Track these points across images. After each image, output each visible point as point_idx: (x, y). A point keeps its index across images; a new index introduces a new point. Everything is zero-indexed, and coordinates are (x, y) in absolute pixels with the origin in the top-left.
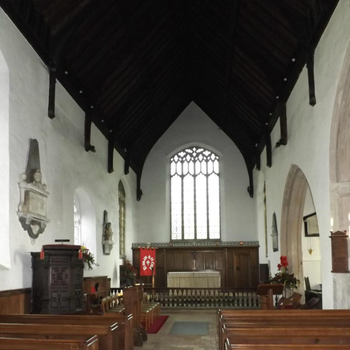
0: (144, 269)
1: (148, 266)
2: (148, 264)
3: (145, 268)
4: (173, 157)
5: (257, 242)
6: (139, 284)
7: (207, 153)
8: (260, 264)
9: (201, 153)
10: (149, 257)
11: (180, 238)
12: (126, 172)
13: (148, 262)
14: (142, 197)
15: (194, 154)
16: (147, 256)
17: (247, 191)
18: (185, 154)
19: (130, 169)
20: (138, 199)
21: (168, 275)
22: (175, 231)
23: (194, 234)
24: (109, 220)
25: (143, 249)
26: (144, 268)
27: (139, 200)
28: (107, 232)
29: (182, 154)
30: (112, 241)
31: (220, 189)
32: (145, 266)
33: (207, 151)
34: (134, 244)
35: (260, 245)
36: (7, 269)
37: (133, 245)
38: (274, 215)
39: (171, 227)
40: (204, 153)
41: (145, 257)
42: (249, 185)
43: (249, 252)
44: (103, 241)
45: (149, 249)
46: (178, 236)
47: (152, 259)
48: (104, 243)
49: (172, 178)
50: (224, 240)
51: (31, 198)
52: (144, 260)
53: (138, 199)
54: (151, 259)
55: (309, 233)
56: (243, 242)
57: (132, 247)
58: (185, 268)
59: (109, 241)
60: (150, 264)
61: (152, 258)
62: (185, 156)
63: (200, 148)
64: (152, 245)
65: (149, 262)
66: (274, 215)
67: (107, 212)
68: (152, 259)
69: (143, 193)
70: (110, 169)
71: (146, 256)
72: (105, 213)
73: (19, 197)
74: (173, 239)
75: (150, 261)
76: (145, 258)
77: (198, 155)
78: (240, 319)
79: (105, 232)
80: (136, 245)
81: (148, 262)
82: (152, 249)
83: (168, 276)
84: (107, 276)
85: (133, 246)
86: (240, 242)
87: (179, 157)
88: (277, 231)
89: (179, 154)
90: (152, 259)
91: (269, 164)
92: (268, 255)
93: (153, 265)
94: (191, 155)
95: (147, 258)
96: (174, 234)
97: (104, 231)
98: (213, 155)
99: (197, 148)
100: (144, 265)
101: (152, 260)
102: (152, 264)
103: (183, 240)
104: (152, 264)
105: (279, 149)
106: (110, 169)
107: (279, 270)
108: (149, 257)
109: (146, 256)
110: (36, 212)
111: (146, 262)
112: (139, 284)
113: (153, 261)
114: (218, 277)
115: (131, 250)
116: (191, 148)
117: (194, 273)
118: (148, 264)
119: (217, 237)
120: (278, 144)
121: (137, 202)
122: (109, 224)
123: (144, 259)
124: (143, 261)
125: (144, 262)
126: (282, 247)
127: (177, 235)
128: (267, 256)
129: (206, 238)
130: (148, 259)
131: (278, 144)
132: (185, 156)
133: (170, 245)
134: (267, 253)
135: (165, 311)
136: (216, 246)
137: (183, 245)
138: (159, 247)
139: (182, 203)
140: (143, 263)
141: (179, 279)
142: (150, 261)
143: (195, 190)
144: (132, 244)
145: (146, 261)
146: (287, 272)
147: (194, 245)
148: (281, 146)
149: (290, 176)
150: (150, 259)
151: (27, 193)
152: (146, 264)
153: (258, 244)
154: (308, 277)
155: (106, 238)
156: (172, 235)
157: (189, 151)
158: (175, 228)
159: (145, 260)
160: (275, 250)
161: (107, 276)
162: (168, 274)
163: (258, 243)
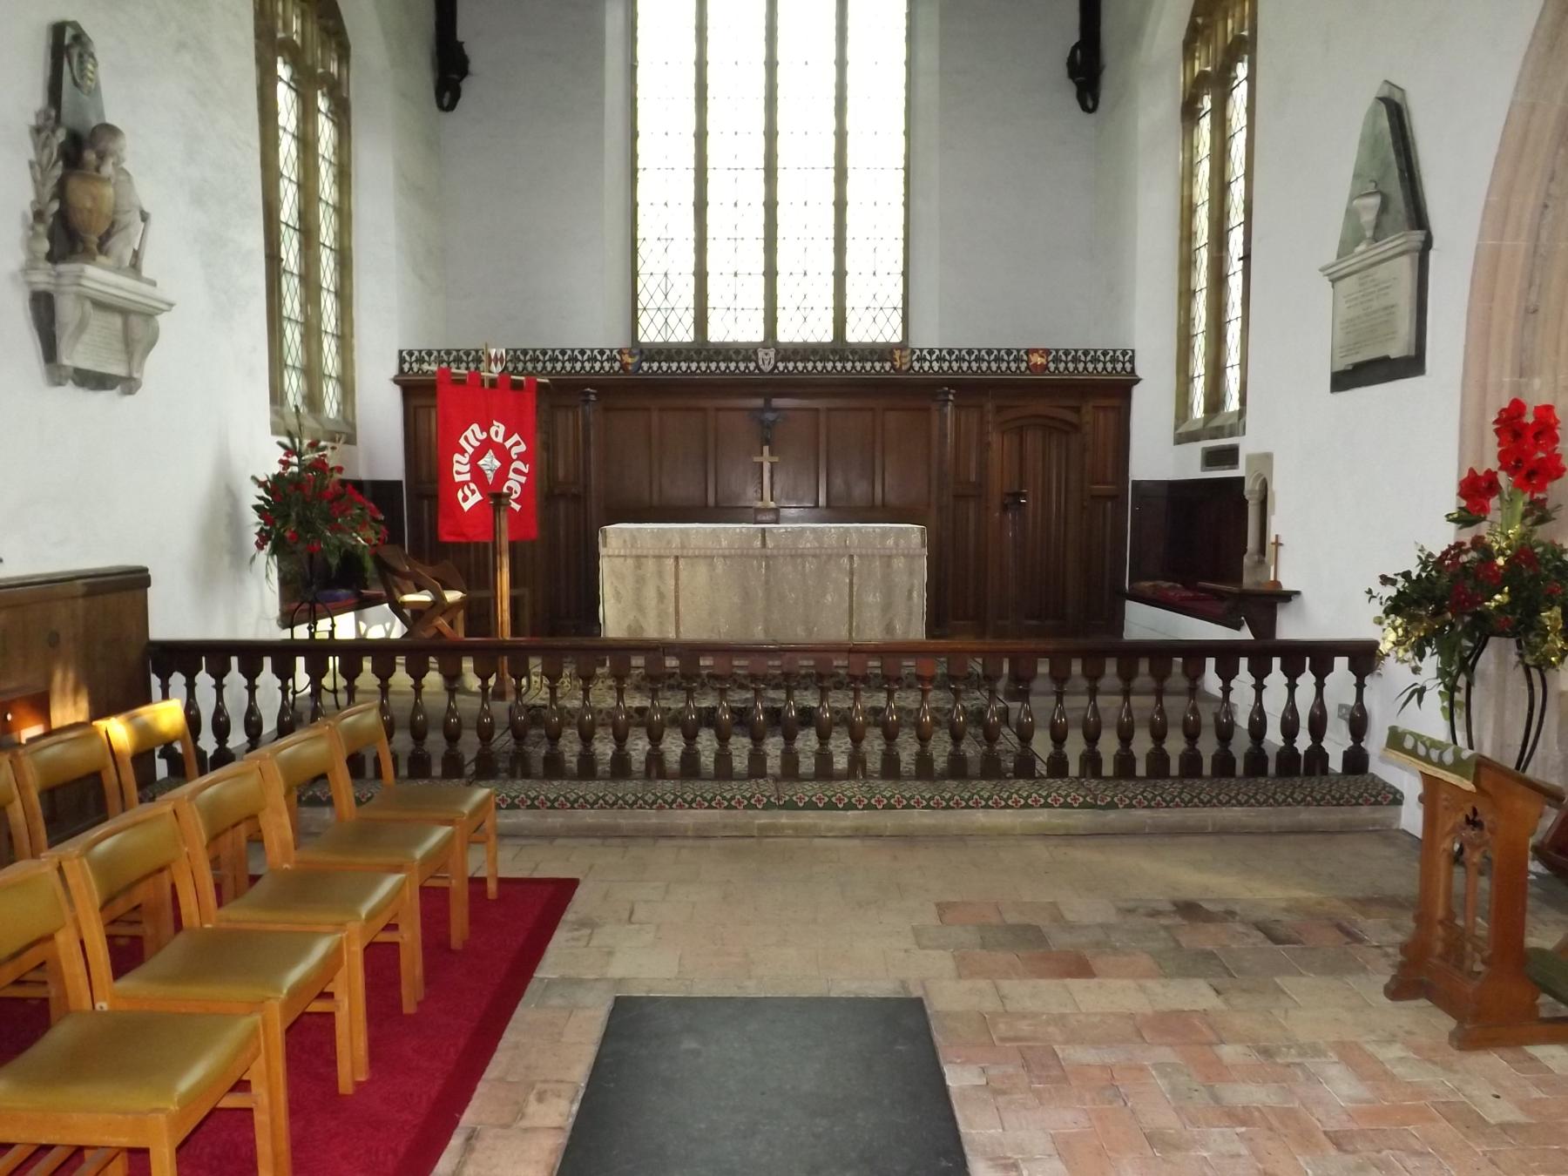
0: (466, 506)
2: (490, 475)
3: (470, 499)
5: (1124, 353)
6: (424, 597)
8: (1137, 484)
10: (493, 430)
11: (683, 334)
13: (490, 463)
14: (468, 86)
16: (485, 427)
17: (1063, 70)
20: (446, 101)
21: (605, 545)
22: (659, 297)
23: (760, 315)
25: (460, 382)
26: (465, 498)
27: (451, 107)
28: (81, 194)
31: (910, 63)
32: (473, 486)
34: (411, 353)
35: (1139, 372)
37: (402, 360)
39: (635, 274)
41: (468, 433)
43: (1077, 410)
44: (30, 267)
45: (493, 382)
46: (673, 320)
47: (517, 443)
48: (42, 279)
50: (928, 337)
52: (463, 452)
54: (508, 444)
56: (1047, 352)
57: (401, 370)
58: (711, 501)
60: (502, 475)
61: (516, 438)
64: (516, 359)
65: (497, 464)
67: (80, 37)
68: (517, 443)
69: (474, 65)
71: (475, 427)
74: (643, 338)
75: (503, 454)
76: (472, 436)
78: (1045, 834)
81: (490, 463)
82: (517, 386)
83: (602, 551)
85: (406, 367)
86: (1028, 352)
93: (523, 479)
96: (652, 313)
97: (51, 184)
100: (467, 477)
102: (511, 475)
103: (701, 349)
104: (517, 471)
108: (498, 430)
109: (475, 427)
112: (424, 597)
113: (521, 457)
114: (910, 557)
115: (395, 393)
117: (764, 529)
118: (490, 475)
119: (888, 331)
121: (443, 115)
123: (462, 442)
124: (457, 457)
125: (465, 459)
129: (828, 337)
130: (486, 446)
133: (623, 366)
138: (559, 373)
139: (701, 65)
140: (456, 467)
141: (671, 561)
142: (503, 454)
143: (771, 65)
144: (401, 352)
145: (479, 453)
146: (1541, 533)
147: (767, 368)
150: (502, 446)
152: (477, 474)
153: (1128, 366)
156: (643, 320)
158: (659, 278)
159: (519, 465)
162: (605, 537)
163: (1132, 360)
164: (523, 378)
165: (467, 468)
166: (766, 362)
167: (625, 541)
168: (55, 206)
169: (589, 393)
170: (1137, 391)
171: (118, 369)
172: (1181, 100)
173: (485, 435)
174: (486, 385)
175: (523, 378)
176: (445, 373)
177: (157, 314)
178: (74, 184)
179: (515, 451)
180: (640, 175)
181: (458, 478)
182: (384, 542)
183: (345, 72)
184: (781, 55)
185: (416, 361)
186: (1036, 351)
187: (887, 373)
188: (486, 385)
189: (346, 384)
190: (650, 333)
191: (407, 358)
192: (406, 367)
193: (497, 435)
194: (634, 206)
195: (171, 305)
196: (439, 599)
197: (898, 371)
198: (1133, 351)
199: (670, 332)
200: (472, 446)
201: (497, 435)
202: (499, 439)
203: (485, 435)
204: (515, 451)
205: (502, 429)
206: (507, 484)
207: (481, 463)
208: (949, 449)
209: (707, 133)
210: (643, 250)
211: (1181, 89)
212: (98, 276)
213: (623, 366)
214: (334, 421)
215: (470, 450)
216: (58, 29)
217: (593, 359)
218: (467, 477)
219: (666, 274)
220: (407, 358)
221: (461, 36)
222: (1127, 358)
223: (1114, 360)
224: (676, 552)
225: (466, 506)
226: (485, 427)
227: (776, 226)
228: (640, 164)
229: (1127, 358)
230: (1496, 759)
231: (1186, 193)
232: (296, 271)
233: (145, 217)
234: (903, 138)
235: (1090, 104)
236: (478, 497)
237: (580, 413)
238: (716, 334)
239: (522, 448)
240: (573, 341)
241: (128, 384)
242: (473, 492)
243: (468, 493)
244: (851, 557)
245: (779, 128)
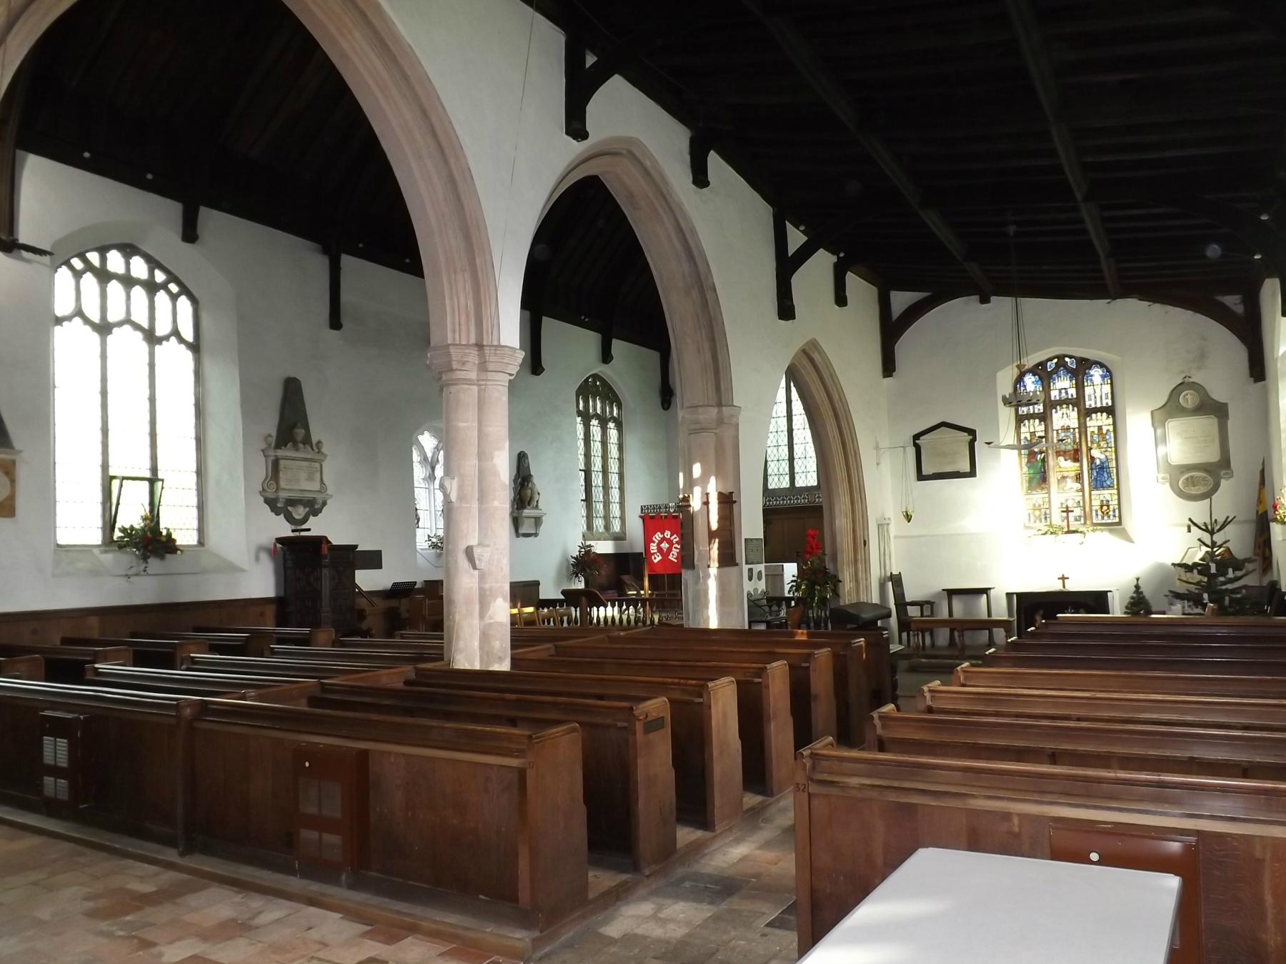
0: (655, 561)
1: (665, 554)
2: (665, 550)
13: (665, 546)
14: (678, 399)
16: (663, 533)
20: (666, 406)
26: (655, 558)
27: (668, 408)
32: (658, 554)
34: (645, 507)
36: (242, 570)
37: (642, 509)
41: (656, 536)
47: (676, 538)
48: (515, 515)
51: (283, 469)
52: (654, 542)
53: (666, 406)
54: (672, 538)
60: (670, 550)
61: (675, 536)
65: (667, 546)
68: (676, 538)
71: (659, 533)
73: (261, 470)
74: (770, 487)
75: (670, 542)
79: (520, 493)
80: (648, 509)
84: (356, 546)
90: (675, 539)
92: (1036, 536)
93: (678, 551)
95: (662, 536)
100: (656, 551)
102: (673, 549)
104: (676, 548)
107: (123, 530)
108: (667, 534)
111: (658, 545)
113: (677, 543)
115: (640, 521)
118: (665, 550)
125: (656, 544)
127: (805, 449)
130: (663, 539)
140: (651, 548)
142: (670, 542)
145: (661, 542)
152: (660, 550)
161: (356, 546)
171: (534, 532)
178: (522, 491)
179: (674, 541)
182: (1208, 495)
189: (623, 518)
195: (545, 514)
197: (810, 503)
202: (669, 537)
204: (674, 541)
205: (669, 533)
212: (527, 512)
214: (618, 533)
215: (657, 541)
216: (519, 454)
218: (656, 551)
225: (655, 561)
226: (663, 533)
230: (883, 626)
232: (601, 485)
233: (539, 494)
236: (660, 558)
239: (677, 539)
241: (536, 535)
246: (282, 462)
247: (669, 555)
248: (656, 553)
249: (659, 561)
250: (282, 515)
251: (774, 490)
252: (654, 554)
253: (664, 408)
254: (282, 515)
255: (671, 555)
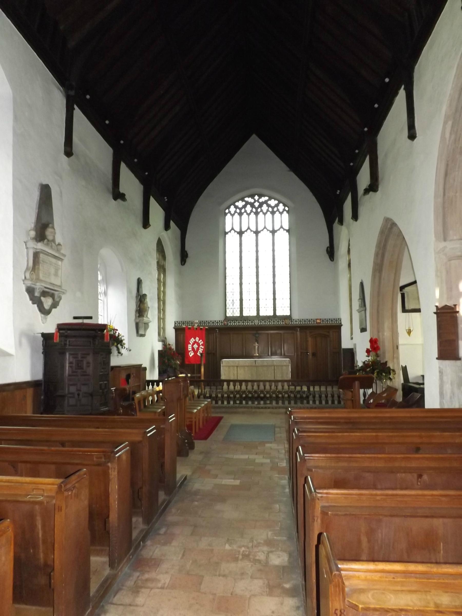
0: (191, 356)
1: (195, 352)
2: (196, 349)
3: (191, 354)
4: (229, 208)
5: (339, 319)
6: (183, 375)
7: (273, 202)
8: (343, 349)
9: (266, 202)
11: (237, 314)
12: (167, 227)
13: (196, 346)
14: (188, 260)
15: (257, 204)
16: (195, 339)
18: (244, 203)
19: (172, 224)
22: (231, 305)
24: (145, 290)
25: (189, 328)
26: (191, 354)
27: (184, 264)
29: (240, 204)
30: (149, 318)
31: (290, 250)
32: (192, 351)
33: (273, 200)
34: (177, 322)
35: (342, 323)
37: (175, 323)
38: (362, 284)
40: (269, 202)
42: (328, 245)
43: (329, 332)
45: (196, 328)
47: (201, 342)
48: (138, 321)
49: (227, 235)
51: (42, 262)
52: (190, 344)
54: (199, 342)
55: (407, 308)
56: (320, 319)
57: (175, 325)
59: (145, 318)
60: (198, 349)
61: (201, 340)
62: (244, 207)
63: (264, 196)
64: (200, 323)
65: (197, 346)
66: (362, 284)
68: (201, 342)
69: (189, 255)
70: (146, 224)
71: (193, 338)
72: (139, 282)
74: (228, 315)
75: (198, 344)
76: (192, 340)
77: (261, 205)
79: (139, 306)
81: (196, 346)
82: (201, 329)
84: (141, 365)
85: (176, 325)
86: (316, 319)
87: (236, 207)
88: (365, 305)
89: (237, 204)
90: (201, 342)
91: (355, 217)
93: (202, 350)
94: (252, 205)
95: (194, 340)
96: (230, 309)
98: (281, 205)
99: (260, 196)
100: (191, 349)
101: (201, 344)
102: (200, 349)
104: (201, 348)
105: (367, 196)
106: (146, 224)
108: (197, 339)
109: (193, 338)
110: (47, 280)
112: (183, 375)
113: (202, 345)
115: (174, 331)
116: (252, 196)
118: (196, 349)
120: (367, 191)
122: (145, 295)
124: (189, 345)
125: (191, 345)
126: (372, 326)
128: (352, 339)
129: (272, 314)
130: (195, 342)
131: (367, 191)
132: (244, 207)
133: (224, 324)
134: (352, 334)
135: (218, 410)
136: (224, 326)
137: (241, 324)
140: (189, 347)
142: (198, 344)
143: (257, 267)
144: (175, 322)
145: (193, 344)
147: (256, 324)
148: (371, 193)
149: (382, 232)
151: (36, 255)
152: (193, 349)
153: (340, 322)
154: (406, 366)
155: (141, 314)
156: (228, 311)
157: (250, 200)
159: (201, 346)
160: (363, 330)
161: (141, 365)
163: (341, 320)
164: (202, 327)
165: (191, 347)
166: (256, 323)
167: (226, 363)
168: (139, 309)
169: (217, 330)
170: (342, 327)
172: (348, 263)
173: (195, 340)
174: (195, 329)
175: (202, 327)
176: (187, 327)
177: (149, 323)
180: (227, 277)
181: (189, 350)
183: (165, 263)
184: (259, 249)
185: (179, 323)
186: (318, 319)
187: (284, 325)
188: (195, 329)
190: (229, 314)
191: (176, 323)
192: (176, 325)
193: (197, 340)
194: (225, 284)
196: (187, 376)
198: (341, 319)
199: (234, 313)
200: (192, 342)
201: (197, 340)
202: (197, 341)
203: (194, 340)
206: (199, 351)
207: (194, 346)
208: (109, 430)
209: (242, 267)
210: (228, 294)
211: (348, 261)
213: (224, 324)
215: (192, 343)
217: (217, 323)
219: (233, 300)
220: (176, 323)
221: (186, 249)
222: (339, 320)
223: (336, 321)
224: (237, 365)
225: (191, 356)
226: (195, 339)
227: (259, 310)
228: (227, 275)
229: (339, 320)
231: (350, 284)
234: (289, 267)
235: (332, 260)
237: (215, 335)
238: (245, 314)
239: (202, 343)
240: (213, 319)
242: (192, 353)
243: (191, 353)
244: (274, 366)
245: (259, 282)
246: (42, 256)
247: (198, 352)
248: (191, 351)
249: (192, 356)
250: (388, 366)
251: (247, 317)
252: (190, 351)
253: (182, 265)
254: (388, 366)
255: (199, 352)
